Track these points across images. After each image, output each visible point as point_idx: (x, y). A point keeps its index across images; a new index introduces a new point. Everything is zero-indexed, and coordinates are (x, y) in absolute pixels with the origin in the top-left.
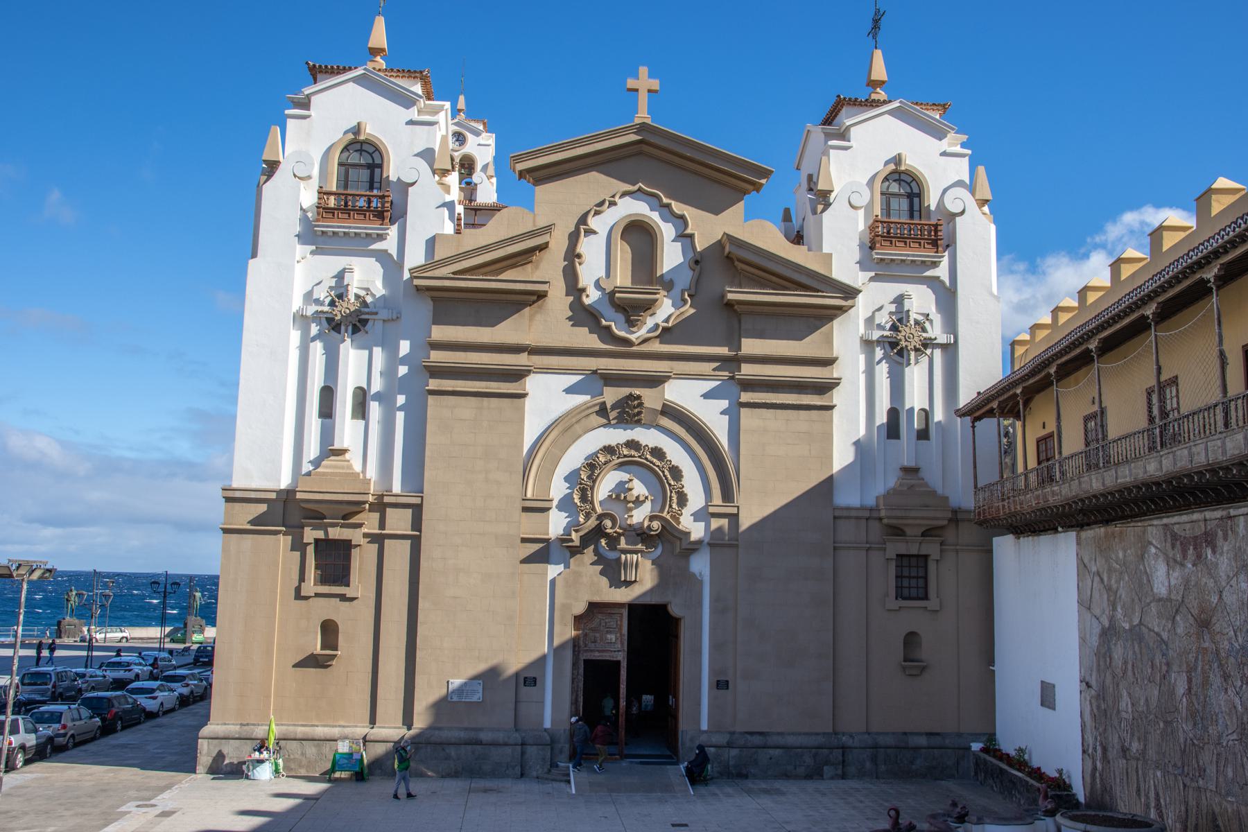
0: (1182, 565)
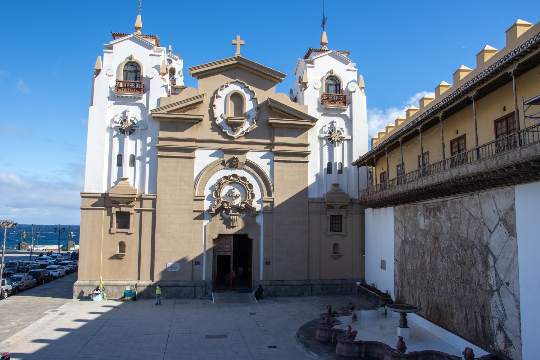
0: (429, 218)
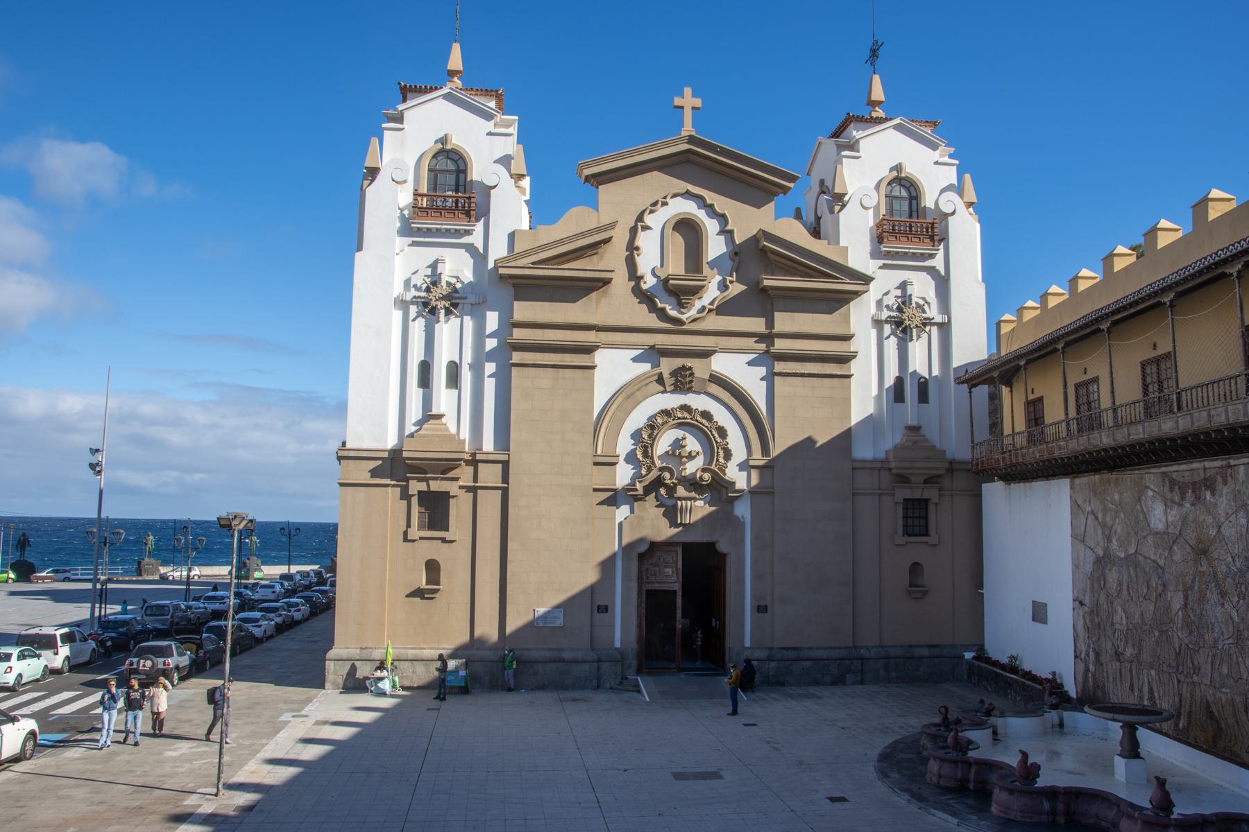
0: (1180, 505)
